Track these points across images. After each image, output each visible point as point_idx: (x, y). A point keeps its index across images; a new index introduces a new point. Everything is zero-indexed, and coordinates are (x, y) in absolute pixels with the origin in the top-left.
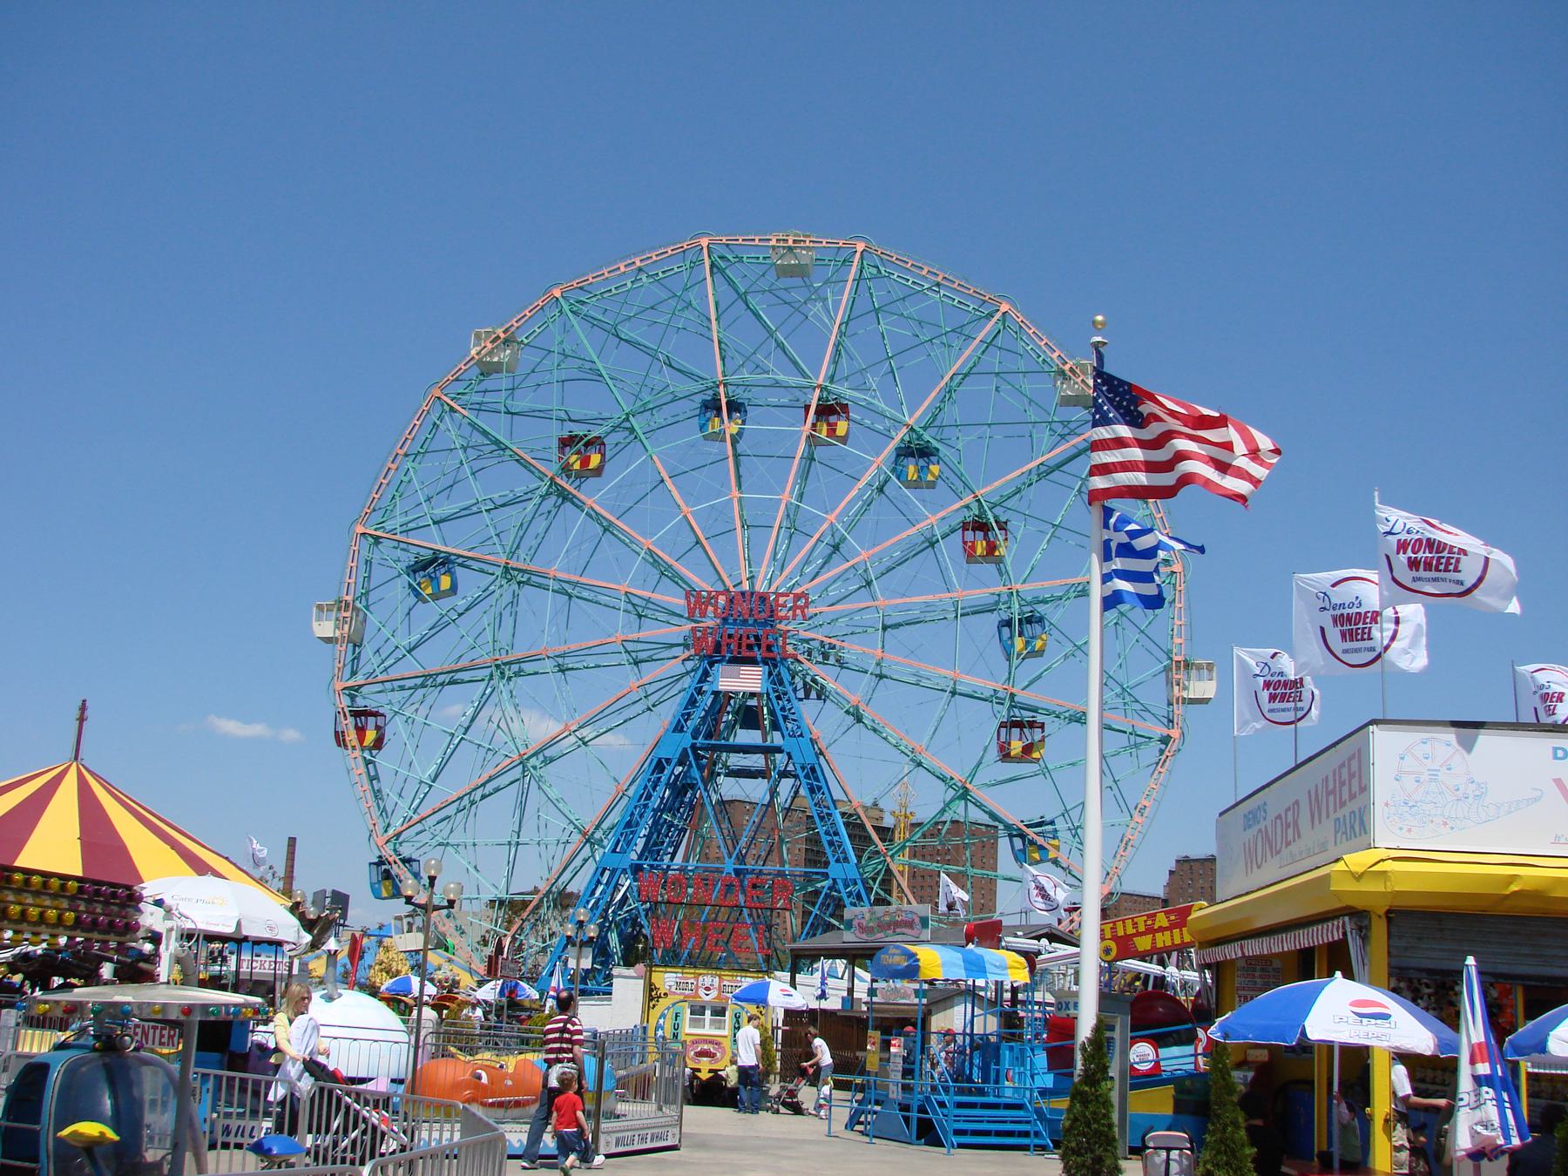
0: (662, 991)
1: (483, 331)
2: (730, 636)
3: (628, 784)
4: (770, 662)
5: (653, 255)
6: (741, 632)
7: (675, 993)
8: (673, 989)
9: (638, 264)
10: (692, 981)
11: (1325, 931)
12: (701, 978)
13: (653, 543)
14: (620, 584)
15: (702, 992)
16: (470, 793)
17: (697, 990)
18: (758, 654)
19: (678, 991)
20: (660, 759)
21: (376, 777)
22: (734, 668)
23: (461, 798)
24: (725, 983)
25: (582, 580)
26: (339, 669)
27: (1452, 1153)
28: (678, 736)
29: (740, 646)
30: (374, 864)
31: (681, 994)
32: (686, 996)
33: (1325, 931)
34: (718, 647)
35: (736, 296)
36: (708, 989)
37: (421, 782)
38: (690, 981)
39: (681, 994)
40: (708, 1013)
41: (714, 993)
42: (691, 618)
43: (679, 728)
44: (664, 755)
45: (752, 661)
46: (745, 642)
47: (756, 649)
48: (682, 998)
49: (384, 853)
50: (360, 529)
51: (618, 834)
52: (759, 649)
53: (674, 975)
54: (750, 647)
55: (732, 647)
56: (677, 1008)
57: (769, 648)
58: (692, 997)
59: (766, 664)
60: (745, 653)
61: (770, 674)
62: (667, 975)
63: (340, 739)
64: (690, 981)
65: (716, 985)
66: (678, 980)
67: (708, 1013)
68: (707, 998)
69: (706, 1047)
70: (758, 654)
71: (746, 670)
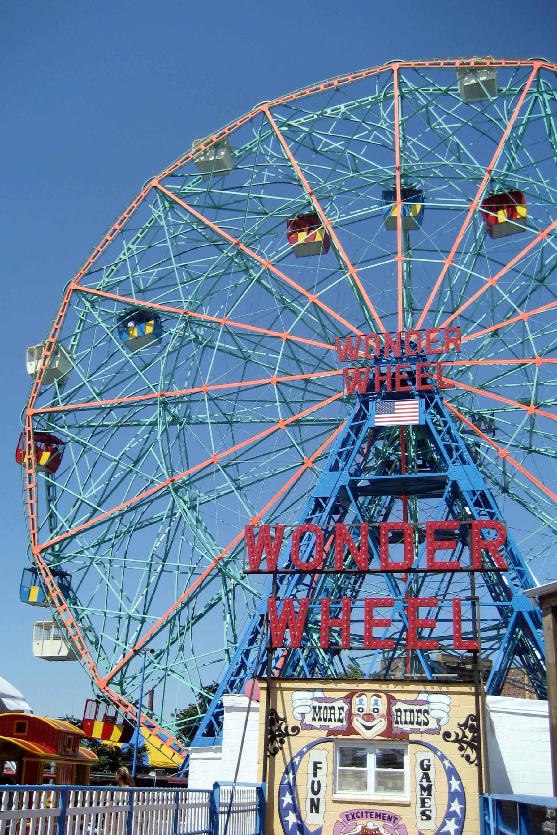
0: (291, 723)
5: (125, 215)
6: (394, 370)
7: (311, 728)
8: (308, 720)
10: (341, 704)
12: (356, 700)
14: (270, 378)
15: (357, 723)
17: (350, 721)
18: (414, 389)
19: (317, 724)
24: (399, 705)
31: (322, 728)
32: (332, 732)
34: (371, 386)
35: (522, 330)
36: (368, 717)
38: (337, 705)
39: (322, 728)
40: (371, 759)
41: (380, 725)
42: (269, 527)
43: (335, 468)
45: (408, 396)
46: (398, 380)
47: (409, 383)
48: (324, 734)
50: (30, 412)
52: (414, 385)
53: (309, 695)
54: (404, 383)
55: (386, 383)
56: (316, 755)
57: (424, 381)
58: (343, 733)
60: (399, 388)
61: (427, 406)
62: (297, 695)
64: (337, 705)
65: (383, 710)
66: (316, 704)
67: (371, 759)
68: (368, 734)
69: (371, 825)
70: (414, 389)
71: (399, 405)
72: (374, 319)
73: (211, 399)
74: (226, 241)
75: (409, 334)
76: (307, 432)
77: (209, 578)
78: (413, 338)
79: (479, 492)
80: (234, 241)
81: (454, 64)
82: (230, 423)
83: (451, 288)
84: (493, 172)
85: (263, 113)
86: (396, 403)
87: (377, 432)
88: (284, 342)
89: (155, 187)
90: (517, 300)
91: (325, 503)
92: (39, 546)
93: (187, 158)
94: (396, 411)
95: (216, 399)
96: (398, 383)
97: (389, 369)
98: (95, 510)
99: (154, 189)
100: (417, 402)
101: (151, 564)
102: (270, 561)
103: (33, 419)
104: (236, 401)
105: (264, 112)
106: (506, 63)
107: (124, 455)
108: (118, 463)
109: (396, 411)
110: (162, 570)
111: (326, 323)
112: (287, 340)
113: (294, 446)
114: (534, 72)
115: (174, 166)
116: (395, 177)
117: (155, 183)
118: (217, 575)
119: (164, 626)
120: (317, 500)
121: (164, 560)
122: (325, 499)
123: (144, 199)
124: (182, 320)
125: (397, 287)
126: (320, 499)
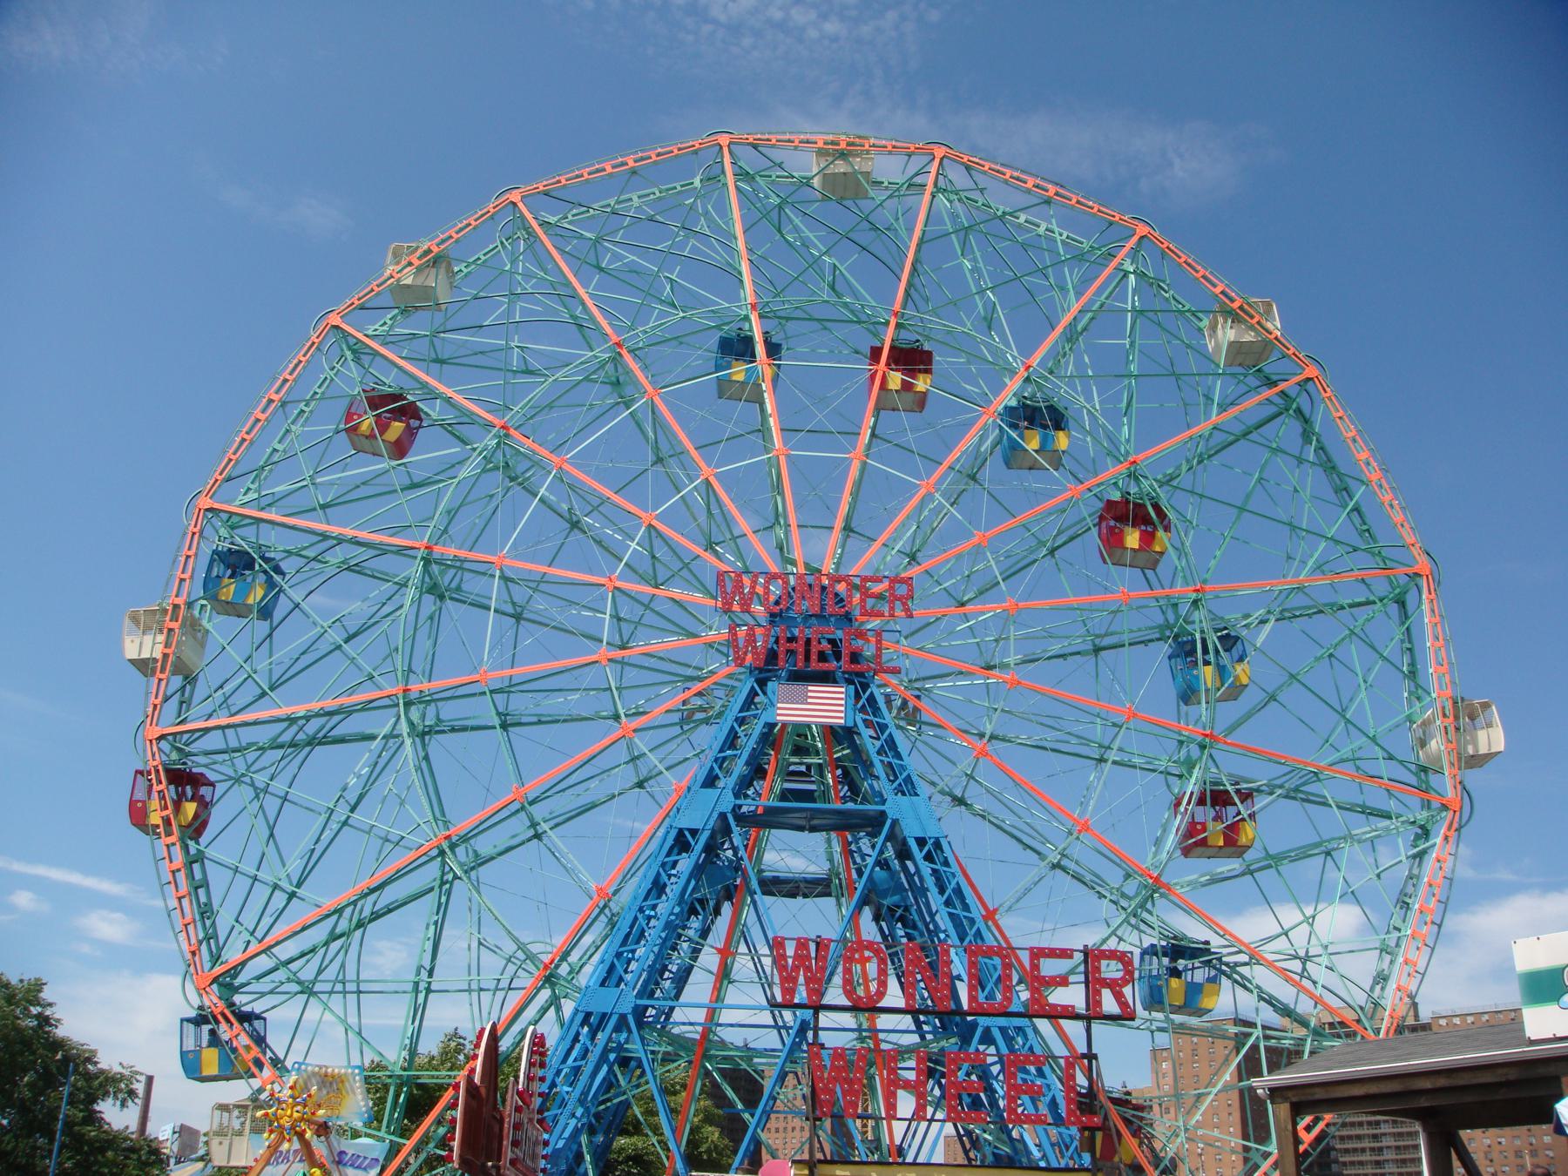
1: (406, 245)
2: (791, 639)
3: (861, 538)
4: (858, 680)
9: (631, 164)
11: (1350, 1145)
13: (657, 517)
16: (355, 903)
20: (681, 831)
21: (205, 884)
22: (796, 688)
23: (339, 911)
25: (521, 671)
26: (155, 706)
27: (126, 1139)
28: (712, 794)
29: (807, 658)
30: (189, 1020)
33: (1350, 1145)
34: (772, 656)
37: (276, 887)
43: (710, 781)
44: (685, 822)
45: (826, 678)
49: (207, 1003)
50: (205, 502)
51: (612, 952)
59: (849, 682)
60: (815, 665)
61: (858, 697)
63: (138, 816)
72: (789, 526)
73: (505, 579)
74: (595, 325)
75: (835, 579)
76: (632, 675)
77: (424, 859)
78: (841, 588)
79: (932, 840)
80: (615, 339)
81: (1026, 183)
82: (518, 617)
83: (919, 522)
84: (1031, 369)
85: (718, 147)
86: (810, 688)
87: (771, 737)
88: (643, 528)
89: (514, 204)
90: (1006, 570)
91: (693, 837)
92: (158, 728)
93: (577, 177)
94: (809, 700)
95: (512, 580)
96: (814, 657)
97: (802, 631)
98: (264, 694)
99: (511, 206)
100: (843, 690)
101: (333, 811)
102: (810, 992)
103: (204, 515)
104: (535, 590)
105: (721, 147)
106: (1099, 211)
107: (338, 623)
108: (326, 631)
109: (809, 700)
110: (345, 823)
111: (715, 511)
112: (650, 526)
113: (610, 689)
114: (1135, 239)
115: (554, 180)
116: (887, 323)
117: (515, 197)
118: (434, 858)
119: (328, 916)
120: (681, 832)
121: (352, 810)
122: (694, 832)
123: (492, 218)
124: (495, 435)
125: (842, 493)
126: (687, 833)
